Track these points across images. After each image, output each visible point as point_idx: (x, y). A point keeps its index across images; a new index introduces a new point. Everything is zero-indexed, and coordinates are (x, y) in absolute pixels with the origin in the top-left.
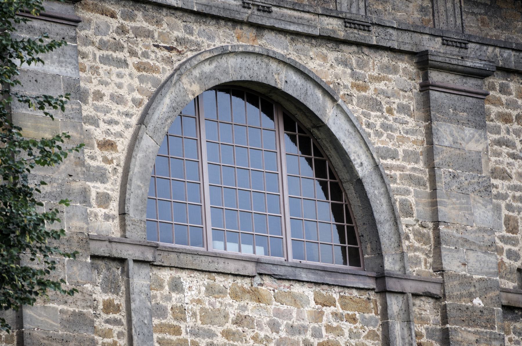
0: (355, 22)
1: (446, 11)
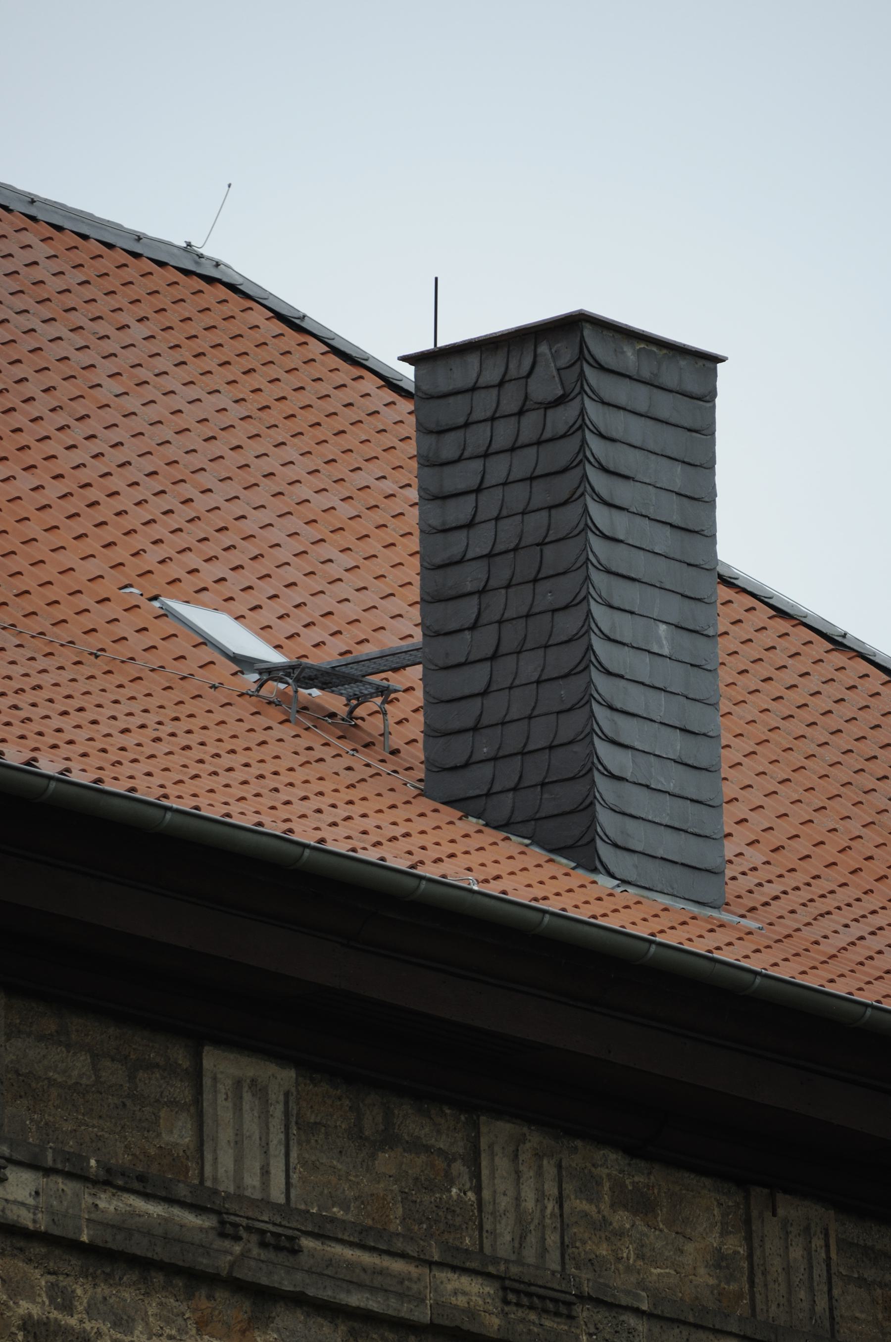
0: (533, 1289)
1: (788, 1269)
